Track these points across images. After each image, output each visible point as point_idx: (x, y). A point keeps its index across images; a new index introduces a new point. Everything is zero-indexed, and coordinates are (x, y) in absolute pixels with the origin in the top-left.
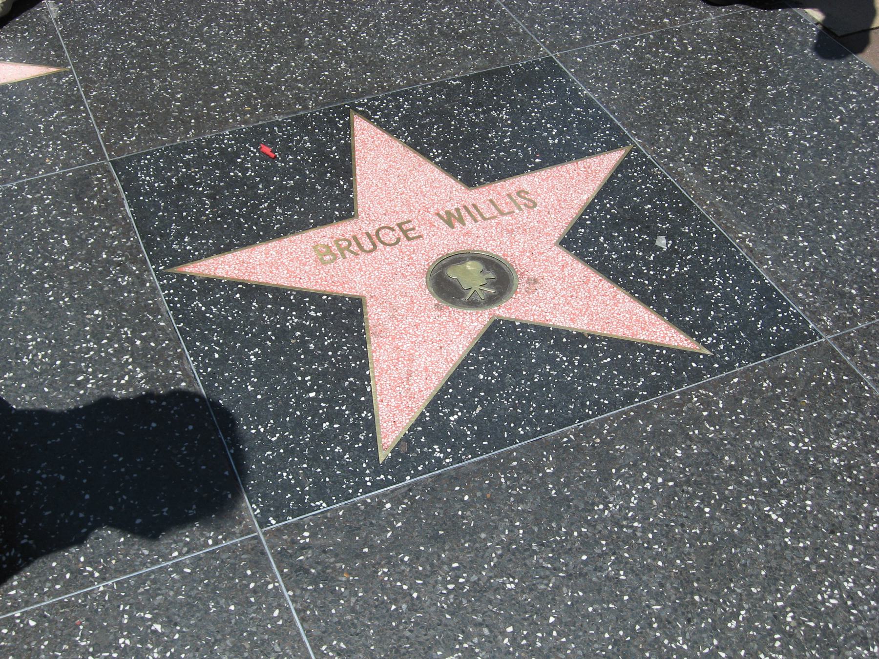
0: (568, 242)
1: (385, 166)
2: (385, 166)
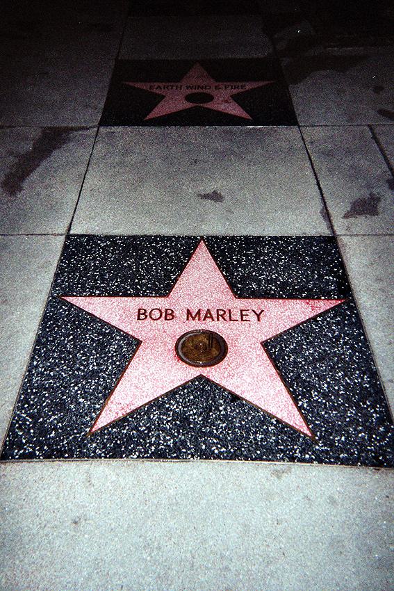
0: (265, 344)
1: (201, 282)
2: (201, 282)
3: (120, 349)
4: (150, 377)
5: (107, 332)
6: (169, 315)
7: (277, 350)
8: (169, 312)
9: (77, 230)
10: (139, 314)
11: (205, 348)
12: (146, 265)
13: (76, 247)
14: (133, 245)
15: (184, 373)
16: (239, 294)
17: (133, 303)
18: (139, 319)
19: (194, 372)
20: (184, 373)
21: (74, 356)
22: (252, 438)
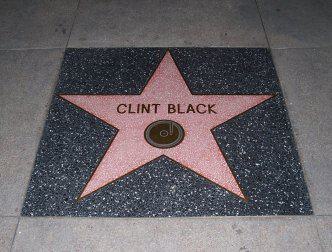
2: (167, 88)
3: (103, 135)
4: (114, 166)
5: (95, 122)
6: (145, 108)
7: (226, 136)
8: (172, 111)
9: (69, 46)
10: (169, 108)
11: (164, 134)
12: (127, 71)
13: (72, 57)
14: (117, 56)
15: (152, 153)
16: (195, 90)
17: (115, 101)
18: (169, 112)
19: (157, 152)
20: (152, 153)
21: (70, 144)
22: (199, 198)
